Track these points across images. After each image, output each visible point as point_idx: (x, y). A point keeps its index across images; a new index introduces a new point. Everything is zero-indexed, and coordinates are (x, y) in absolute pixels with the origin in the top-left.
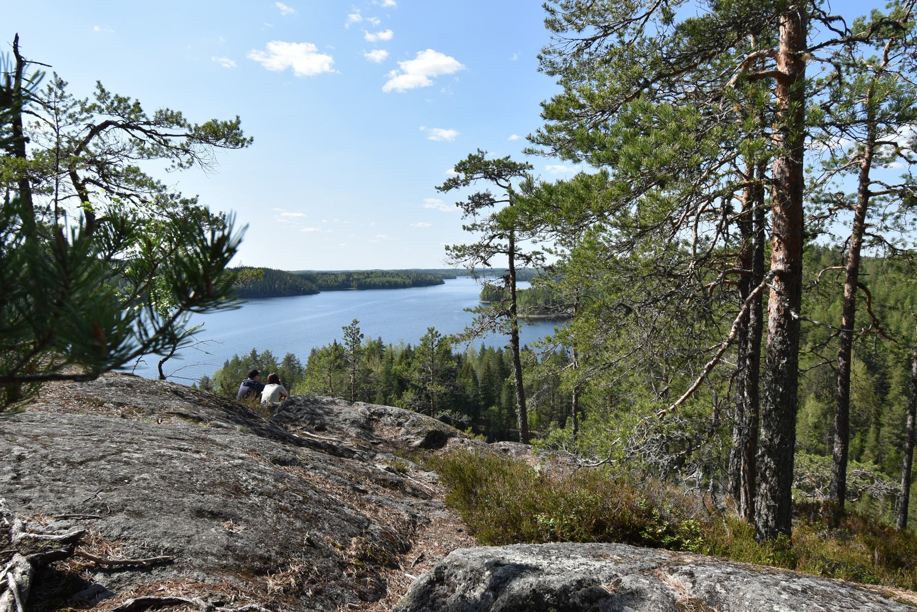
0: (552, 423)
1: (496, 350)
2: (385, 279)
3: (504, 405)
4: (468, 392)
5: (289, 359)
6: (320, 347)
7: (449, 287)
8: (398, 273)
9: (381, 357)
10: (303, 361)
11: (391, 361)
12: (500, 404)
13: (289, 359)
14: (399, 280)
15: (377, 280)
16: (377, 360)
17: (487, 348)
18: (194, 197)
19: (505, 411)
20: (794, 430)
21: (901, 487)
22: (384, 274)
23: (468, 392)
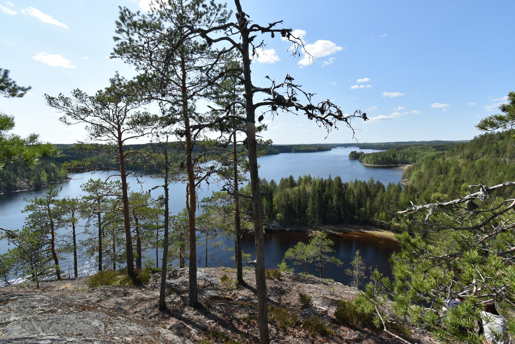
0: (393, 219)
1: (362, 181)
2: (306, 148)
3: (368, 208)
4: (350, 201)
5: (272, 181)
6: (285, 178)
7: (333, 152)
8: (312, 146)
9: (311, 183)
10: (278, 183)
11: (315, 185)
12: (365, 207)
13: (272, 181)
14: (312, 148)
15: (303, 149)
16: (309, 184)
17: (358, 181)
18: (116, 74)
19: (369, 211)
20: (254, 114)
21: (233, 181)
22: (305, 146)
23: (350, 201)
